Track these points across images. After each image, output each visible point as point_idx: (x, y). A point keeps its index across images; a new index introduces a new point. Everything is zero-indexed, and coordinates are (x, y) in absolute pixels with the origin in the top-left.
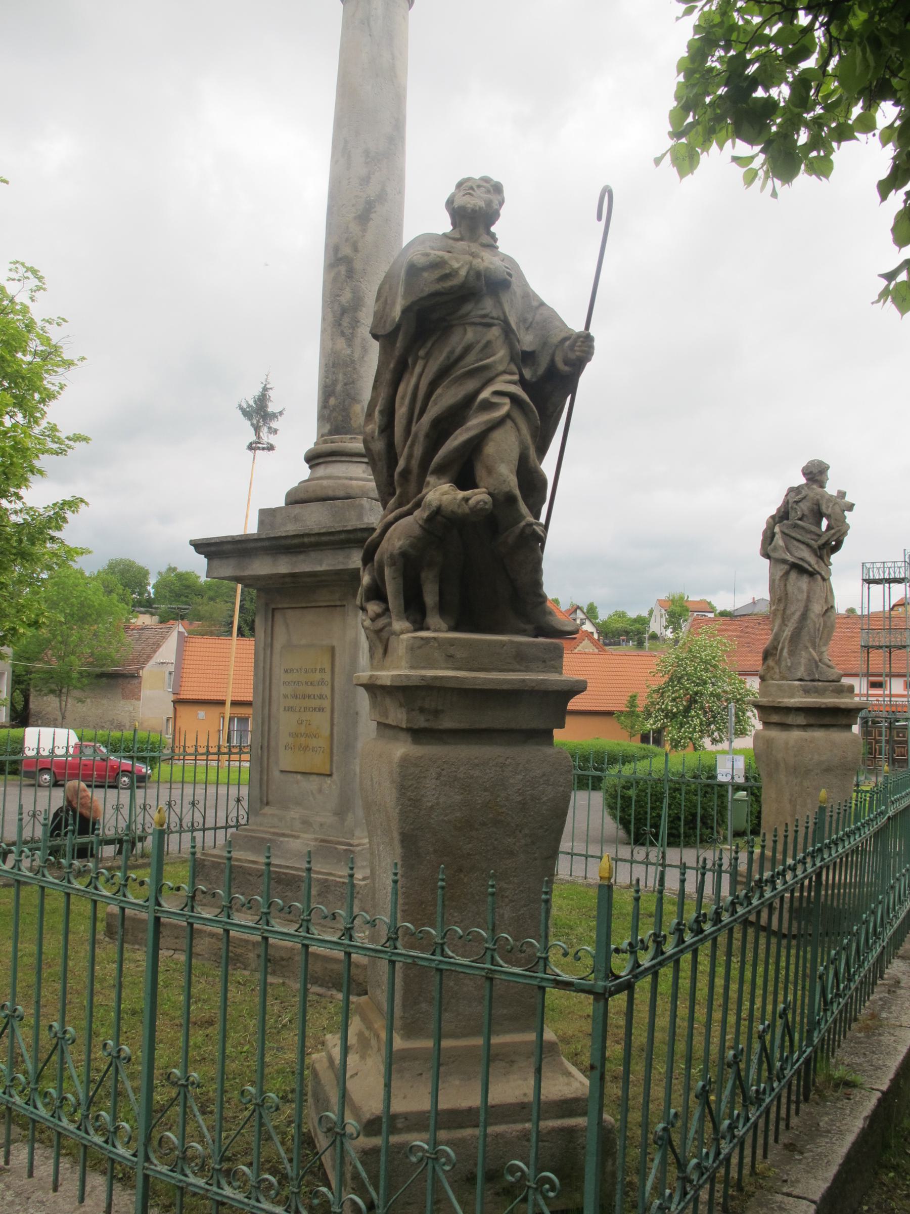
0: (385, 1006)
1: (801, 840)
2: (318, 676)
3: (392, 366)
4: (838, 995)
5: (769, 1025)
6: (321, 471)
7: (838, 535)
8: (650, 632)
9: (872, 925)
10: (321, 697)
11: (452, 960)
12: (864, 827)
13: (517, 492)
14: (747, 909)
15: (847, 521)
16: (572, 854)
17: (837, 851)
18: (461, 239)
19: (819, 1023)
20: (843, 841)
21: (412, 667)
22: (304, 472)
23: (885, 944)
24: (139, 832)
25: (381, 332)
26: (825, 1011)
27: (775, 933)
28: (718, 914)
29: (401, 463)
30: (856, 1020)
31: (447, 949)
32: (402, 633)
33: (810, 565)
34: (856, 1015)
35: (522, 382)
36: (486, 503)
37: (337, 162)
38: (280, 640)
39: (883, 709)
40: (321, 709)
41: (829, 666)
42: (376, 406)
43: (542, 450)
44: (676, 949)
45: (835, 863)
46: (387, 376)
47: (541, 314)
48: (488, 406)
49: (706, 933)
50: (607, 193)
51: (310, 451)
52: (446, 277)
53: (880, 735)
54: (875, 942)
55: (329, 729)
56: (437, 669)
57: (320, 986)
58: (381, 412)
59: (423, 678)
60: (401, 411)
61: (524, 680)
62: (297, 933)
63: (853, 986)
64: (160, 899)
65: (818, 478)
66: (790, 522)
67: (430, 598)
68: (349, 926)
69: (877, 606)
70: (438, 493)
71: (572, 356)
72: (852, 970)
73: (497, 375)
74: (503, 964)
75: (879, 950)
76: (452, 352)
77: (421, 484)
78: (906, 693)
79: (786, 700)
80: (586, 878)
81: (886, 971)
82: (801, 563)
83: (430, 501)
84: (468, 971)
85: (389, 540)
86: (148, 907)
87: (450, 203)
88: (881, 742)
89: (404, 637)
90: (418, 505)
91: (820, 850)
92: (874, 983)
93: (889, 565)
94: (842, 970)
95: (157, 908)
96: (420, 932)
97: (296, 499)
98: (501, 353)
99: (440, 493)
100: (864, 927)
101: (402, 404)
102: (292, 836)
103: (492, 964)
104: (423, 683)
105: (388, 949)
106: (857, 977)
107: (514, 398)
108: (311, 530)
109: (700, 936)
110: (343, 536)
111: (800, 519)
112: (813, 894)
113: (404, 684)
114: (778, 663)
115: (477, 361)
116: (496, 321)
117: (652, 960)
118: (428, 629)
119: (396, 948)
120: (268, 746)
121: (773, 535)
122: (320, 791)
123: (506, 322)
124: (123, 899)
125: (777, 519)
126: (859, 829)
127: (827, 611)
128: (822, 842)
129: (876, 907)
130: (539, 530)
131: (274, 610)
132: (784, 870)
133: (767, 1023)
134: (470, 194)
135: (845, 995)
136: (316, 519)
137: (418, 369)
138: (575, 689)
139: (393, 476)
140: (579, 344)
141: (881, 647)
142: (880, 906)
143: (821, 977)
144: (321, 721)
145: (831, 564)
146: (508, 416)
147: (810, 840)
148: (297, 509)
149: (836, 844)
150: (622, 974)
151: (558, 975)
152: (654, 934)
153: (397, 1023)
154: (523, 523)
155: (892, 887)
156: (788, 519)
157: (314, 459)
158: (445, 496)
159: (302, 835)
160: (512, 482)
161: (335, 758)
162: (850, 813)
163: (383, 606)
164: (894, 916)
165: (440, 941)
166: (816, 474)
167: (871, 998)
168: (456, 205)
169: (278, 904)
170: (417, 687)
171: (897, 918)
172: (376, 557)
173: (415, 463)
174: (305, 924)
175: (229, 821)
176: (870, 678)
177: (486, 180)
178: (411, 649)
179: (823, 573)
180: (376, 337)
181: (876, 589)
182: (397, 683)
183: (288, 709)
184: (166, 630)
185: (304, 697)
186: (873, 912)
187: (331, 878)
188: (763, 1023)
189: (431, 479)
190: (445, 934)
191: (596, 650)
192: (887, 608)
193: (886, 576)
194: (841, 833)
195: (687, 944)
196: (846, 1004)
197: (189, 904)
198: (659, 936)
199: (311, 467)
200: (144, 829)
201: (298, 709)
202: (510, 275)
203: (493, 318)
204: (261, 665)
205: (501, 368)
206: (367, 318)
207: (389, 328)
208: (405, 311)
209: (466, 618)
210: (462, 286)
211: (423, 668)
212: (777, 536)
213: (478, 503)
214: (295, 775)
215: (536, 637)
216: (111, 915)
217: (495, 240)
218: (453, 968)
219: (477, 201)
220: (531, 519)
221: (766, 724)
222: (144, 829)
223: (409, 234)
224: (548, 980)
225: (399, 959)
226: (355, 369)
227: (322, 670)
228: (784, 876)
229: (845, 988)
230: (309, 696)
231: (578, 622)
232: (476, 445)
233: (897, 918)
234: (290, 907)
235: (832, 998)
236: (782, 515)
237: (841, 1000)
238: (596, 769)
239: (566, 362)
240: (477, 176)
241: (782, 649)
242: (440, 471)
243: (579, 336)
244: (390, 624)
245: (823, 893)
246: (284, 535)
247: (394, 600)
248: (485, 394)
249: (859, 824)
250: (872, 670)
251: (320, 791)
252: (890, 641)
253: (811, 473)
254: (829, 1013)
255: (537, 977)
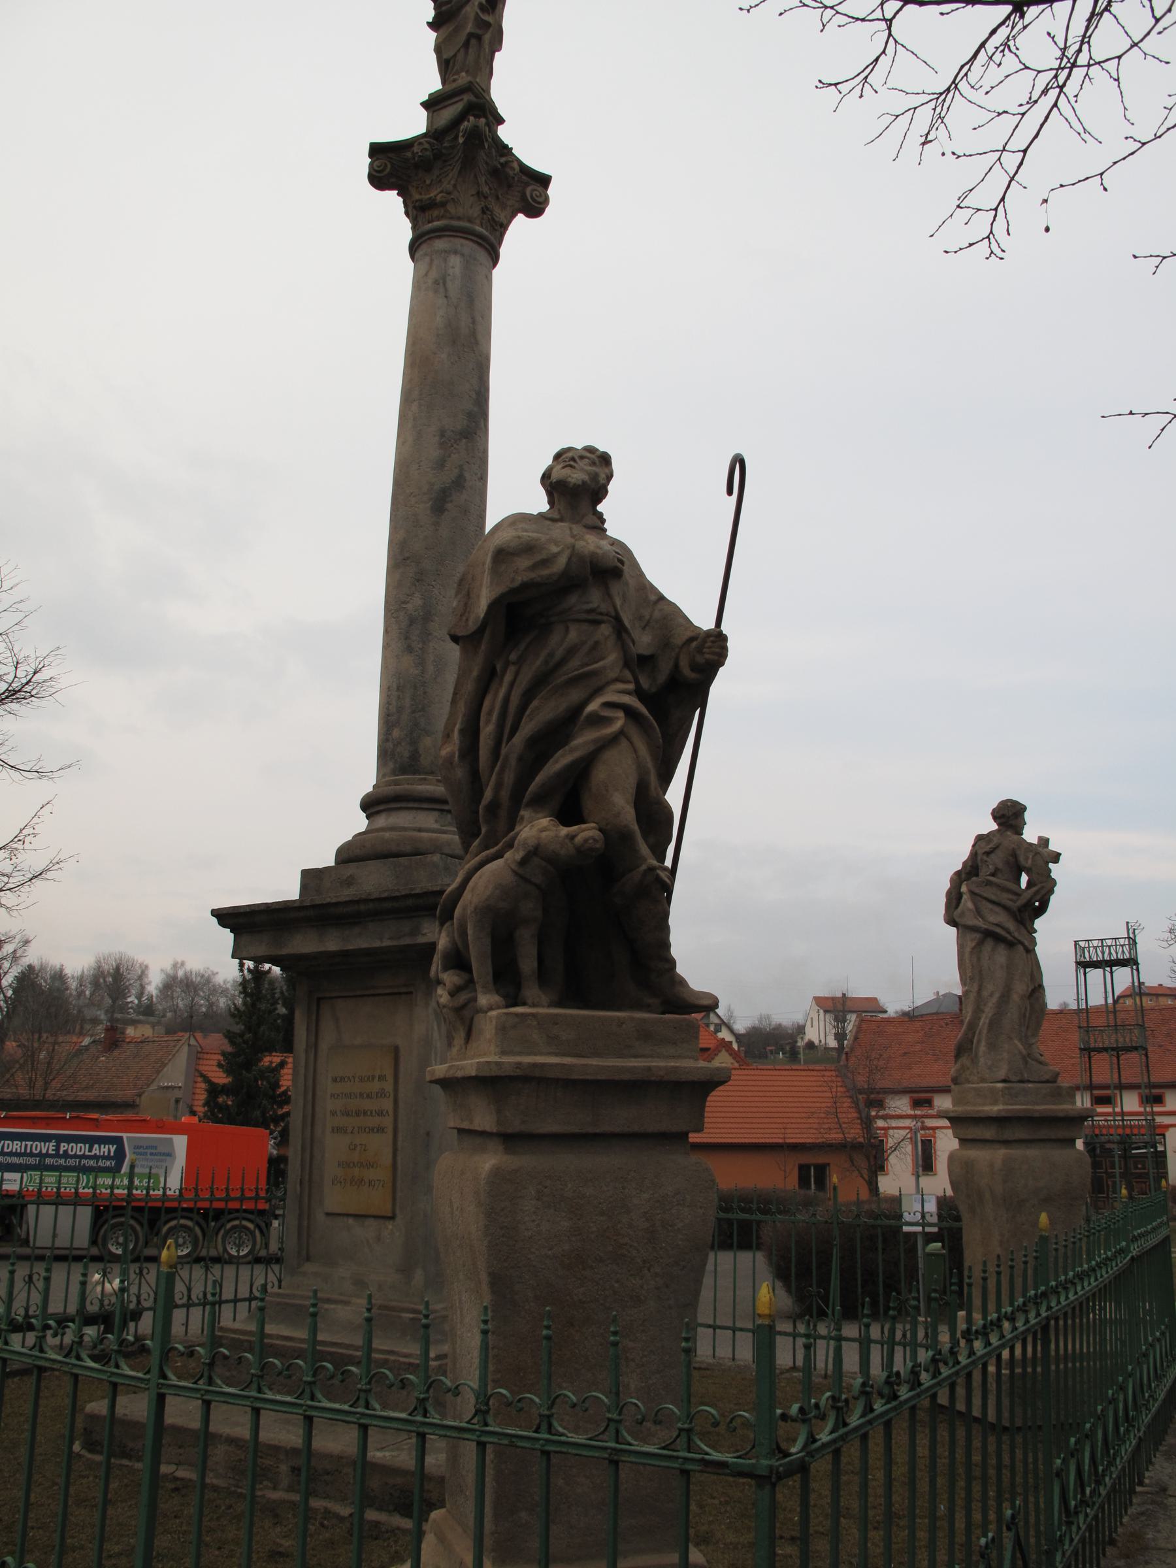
0: (471, 1521)
1: (1018, 1282)
2: (376, 1086)
3: (475, 673)
4: (1084, 1503)
5: (993, 1539)
6: (382, 821)
7: (1043, 892)
8: (806, 1040)
9: (1121, 1406)
10: (381, 1113)
11: (563, 1438)
12: (1100, 1268)
13: (635, 827)
14: (953, 1370)
15: (1053, 875)
16: (714, 1327)
17: (1067, 1298)
18: (561, 520)
19: (1061, 1540)
20: (1074, 1284)
21: (503, 1053)
22: (360, 823)
23: (1141, 1434)
24: (132, 1306)
25: (460, 633)
26: (1069, 1524)
27: (993, 1426)
28: (915, 1373)
29: (488, 794)
30: (1112, 1542)
31: (555, 1424)
32: (491, 1009)
33: (1009, 933)
34: (1110, 1535)
35: (639, 693)
36: (595, 840)
37: (404, 443)
38: (327, 1039)
39: (1112, 1131)
40: (381, 1130)
41: (1041, 1063)
42: (455, 725)
43: (666, 777)
44: (862, 1420)
45: (1066, 1314)
46: (469, 687)
47: (661, 610)
48: (597, 720)
49: (902, 1399)
50: (739, 462)
51: (368, 796)
52: (545, 562)
53: (1113, 1167)
54: (1127, 1431)
55: (390, 1156)
56: (535, 1055)
57: (377, 1509)
58: (461, 731)
59: (518, 1065)
60: (487, 730)
61: (649, 1069)
62: (353, 1409)
63: (1103, 1492)
64: (165, 1368)
65: (1013, 822)
66: (979, 879)
67: (528, 964)
68: (422, 1396)
69: (1096, 998)
70: (535, 829)
71: (700, 659)
72: (1101, 1468)
73: (608, 683)
74: (633, 1442)
75: (1134, 1442)
76: (551, 655)
77: (513, 821)
78: (1142, 1109)
79: (987, 1108)
80: (734, 1359)
81: (1147, 1474)
82: (998, 930)
83: (525, 839)
84: (585, 1453)
85: (473, 890)
86: (148, 1380)
87: (546, 478)
88: (1114, 1176)
89: (494, 1013)
90: (510, 846)
91: (1044, 1294)
92: (1132, 1492)
93: (1109, 942)
94: (1087, 1467)
95: (161, 1381)
96: (519, 1401)
97: (349, 855)
98: (611, 658)
99: (537, 828)
100: (1111, 1407)
101: (488, 722)
102: (341, 1302)
103: (617, 1442)
104: (519, 1072)
105: (476, 1427)
106: (1107, 1479)
107: (629, 711)
108: (369, 894)
109: (894, 1403)
110: (410, 902)
111: (993, 875)
112: (1039, 1369)
113: (493, 1074)
114: (975, 1061)
115: (582, 666)
116: (605, 618)
117: (831, 1432)
118: (524, 1004)
119: (486, 1425)
120: (310, 1181)
121: (960, 896)
122: (379, 1239)
123: (618, 619)
124: (115, 1370)
125: (963, 876)
126: (1094, 1270)
127: (1033, 991)
128: (1047, 1285)
129: (1125, 1380)
130: (664, 875)
131: (319, 999)
132: (999, 1319)
133: (990, 1535)
134: (571, 466)
135: (1094, 1503)
136: (375, 880)
137: (508, 678)
138: (716, 1079)
139: (477, 812)
140: (709, 644)
141: (1105, 1050)
142: (1131, 1380)
143: (1058, 1475)
144: (380, 1145)
145: (1035, 931)
146: (622, 732)
147: (1030, 1281)
148: (351, 869)
149: (1066, 1289)
150: (793, 1450)
151: (707, 1454)
152: (833, 1397)
153: (488, 1542)
154: (644, 867)
155: (1145, 1355)
156: (977, 875)
157: (370, 805)
158: (544, 834)
159: (354, 1300)
160: (628, 815)
161: (399, 1194)
162: (1081, 1248)
163: (465, 976)
164: (1150, 1396)
165: (546, 1412)
166: (1010, 815)
167: (1129, 1512)
168: (555, 477)
169: (327, 1369)
170: (511, 1079)
171: (1155, 1400)
172: (457, 912)
173: (505, 794)
174: (363, 1395)
175: (254, 1290)
176: (1096, 1092)
177: (590, 450)
178: (502, 1029)
179: (1026, 943)
180: (455, 639)
181: (1095, 975)
182: (486, 1073)
183: (336, 1130)
184: (173, 1044)
185: (358, 1114)
186: (1122, 1388)
187: (392, 1358)
188: (985, 1536)
189: (525, 813)
190: (553, 1403)
191: (736, 1065)
192: (1110, 1001)
193: (1106, 957)
194: (1071, 1274)
195: (876, 1413)
196: (1096, 1517)
197: (206, 1374)
198: (839, 1400)
199: (368, 817)
200: (139, 1302)
201: (349, 1130)
202: (622, 562)
203: (601, 614)
204: (302, 1071)
205: (613, 675)
206: (440, 630)
207: (472, 626)
208: (492, 606)
209: (575, 992)
210: (565, 573)
211: (520, 1053)
212: (965, 897)
213: (586, 841)
214: (345, 1219)
215: (663, 1013)
216: (93, 1417)
217: (603, 521)
218: (564, 1450)
219: (576, 476)
220: (655, 863)
221: (963, 1141)
222: (139, 1302)
223: (494, 515)
224: (692, 1460)
225: (491, 1440)
226: (425, 693)
227: (382, 1078)
228: (1000, 1327)
229: (1093, 1492)
230: (365, 1113)
231: (712, 1028)
232: (582, 771)
233: (1155, 1400)
234: (342, 1374)
235: (1076, 1507)
236: (970, 871)
237: (1088, 1510)
238: (743, 1210)
239: (694, 667)
240: (579, 446)
241: (979, 1041)
242: (538, 802)
243: (708, 633)
244: (475, 999)
245: (1053, 1367)
246: (334, 901)
247: (481, 967)
248: (593, 707)
249: (1093, 1263)
250: (1097, 1080)
251: (379, 1239)
252: (1117, 1041)
253: (1003, 816)
254: (1074, 1528)
255: (678, 1458)
